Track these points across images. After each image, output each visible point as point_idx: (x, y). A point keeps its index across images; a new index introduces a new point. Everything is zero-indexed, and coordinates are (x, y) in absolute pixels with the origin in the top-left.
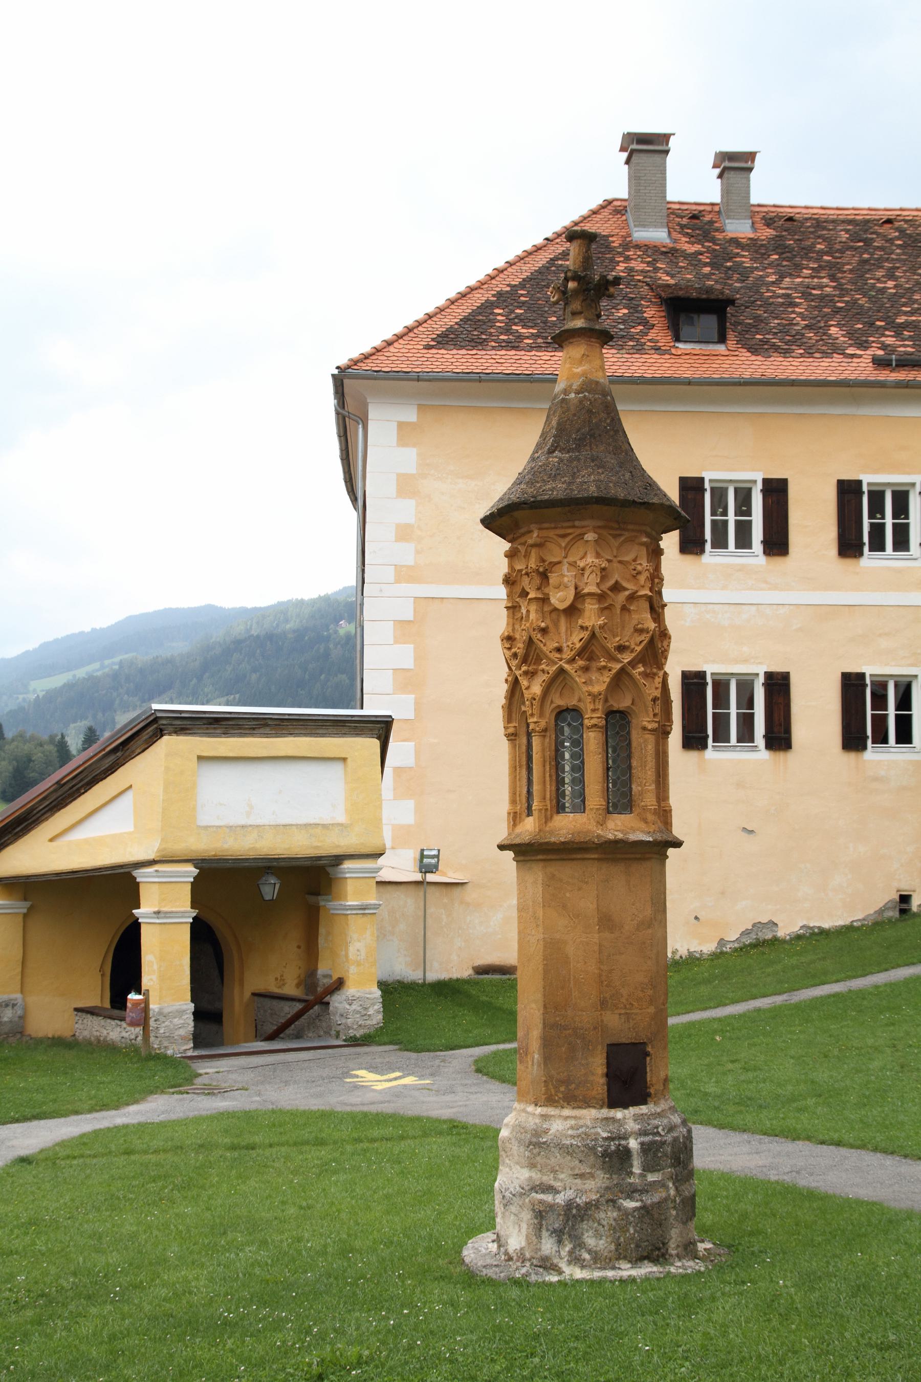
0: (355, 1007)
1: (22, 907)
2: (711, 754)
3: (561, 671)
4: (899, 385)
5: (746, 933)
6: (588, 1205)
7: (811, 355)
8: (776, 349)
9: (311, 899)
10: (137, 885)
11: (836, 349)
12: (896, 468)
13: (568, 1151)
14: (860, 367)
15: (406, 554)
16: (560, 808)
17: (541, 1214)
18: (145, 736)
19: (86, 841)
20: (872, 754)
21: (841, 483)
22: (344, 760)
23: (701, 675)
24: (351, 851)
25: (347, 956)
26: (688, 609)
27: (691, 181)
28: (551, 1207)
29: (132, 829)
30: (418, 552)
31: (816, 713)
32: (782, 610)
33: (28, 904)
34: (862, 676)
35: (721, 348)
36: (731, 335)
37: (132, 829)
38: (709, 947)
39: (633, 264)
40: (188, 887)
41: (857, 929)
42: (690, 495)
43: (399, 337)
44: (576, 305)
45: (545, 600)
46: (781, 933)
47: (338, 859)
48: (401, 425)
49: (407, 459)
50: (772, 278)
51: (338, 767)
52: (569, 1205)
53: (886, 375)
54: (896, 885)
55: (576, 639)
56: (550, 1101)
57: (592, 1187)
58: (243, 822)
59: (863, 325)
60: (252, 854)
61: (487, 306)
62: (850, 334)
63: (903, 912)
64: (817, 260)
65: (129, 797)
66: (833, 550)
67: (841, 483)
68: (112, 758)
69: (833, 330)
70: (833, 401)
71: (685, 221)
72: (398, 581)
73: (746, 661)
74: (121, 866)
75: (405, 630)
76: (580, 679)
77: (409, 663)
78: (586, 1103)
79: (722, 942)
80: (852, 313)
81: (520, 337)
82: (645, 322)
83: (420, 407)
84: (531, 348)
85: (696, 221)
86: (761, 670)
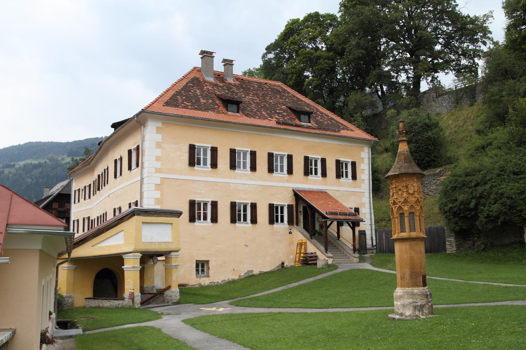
0: (174, 294)
1: (73, 267)
2: (237, 224)
3: (400, 206)
5: (246, 273)
6: (424, 305)
7: (219, 113)
8: (252, 116)
10: (123, 259)
11: (265, 118)
12: (281, 151)
13: (419, 295)
14: (272, 123)
15: (158, 165)
16: (411, 231)
17: (415, 307)
18: (129, 216)
19: (106, 246)
20: (276, 225)
21: (231, 149)
22: (172, 224)
23: (235, 203)
25: (172, 280)
26: (232, 185)
27: (218, 67)
28: (417, 306)
29: (123, 242)
30: (161, 164)
31: (263, 214)
32: (255, 186)
35: (238, 114)
36: (240, 111)
37: (123, 242)
38: (237, 278)
39: (208, 87)
40: (139, 260)
41: (274, 271)
42: (233, 154)
43: (155, 102)
44: (404, 135)
45: (408, 191)
46: (254, 273)
48: (157, 128)
49: (159, 137)
50: (243, 96)
51: (170, 226)
52: (421, 305)
53: (279, 126)
54: (281, 260)
55: (414, 199)
56: (413, 286)
57: (424, 302)
58: (150, 241)
59: (271, 112)
60: (153, 250)
61: (174, 95)
62: (267, 114)
63: (282, 267)
64: (252, 92)
66: (267, 171)
68: (117, 222)
69: (263, 112)
70: (267, 132)
72: (156, 172)
73: (246, 199)
74: (119, 254)
75: (158, 187)
76: (403, 207)
77: (159, 196)
78: (420, 286)
79: (240, 276)
80: (266, 109)
82: (217, 105)
83: (162, 123)
84: (191, 109)
85: (219, 76)
86: (250, 202)
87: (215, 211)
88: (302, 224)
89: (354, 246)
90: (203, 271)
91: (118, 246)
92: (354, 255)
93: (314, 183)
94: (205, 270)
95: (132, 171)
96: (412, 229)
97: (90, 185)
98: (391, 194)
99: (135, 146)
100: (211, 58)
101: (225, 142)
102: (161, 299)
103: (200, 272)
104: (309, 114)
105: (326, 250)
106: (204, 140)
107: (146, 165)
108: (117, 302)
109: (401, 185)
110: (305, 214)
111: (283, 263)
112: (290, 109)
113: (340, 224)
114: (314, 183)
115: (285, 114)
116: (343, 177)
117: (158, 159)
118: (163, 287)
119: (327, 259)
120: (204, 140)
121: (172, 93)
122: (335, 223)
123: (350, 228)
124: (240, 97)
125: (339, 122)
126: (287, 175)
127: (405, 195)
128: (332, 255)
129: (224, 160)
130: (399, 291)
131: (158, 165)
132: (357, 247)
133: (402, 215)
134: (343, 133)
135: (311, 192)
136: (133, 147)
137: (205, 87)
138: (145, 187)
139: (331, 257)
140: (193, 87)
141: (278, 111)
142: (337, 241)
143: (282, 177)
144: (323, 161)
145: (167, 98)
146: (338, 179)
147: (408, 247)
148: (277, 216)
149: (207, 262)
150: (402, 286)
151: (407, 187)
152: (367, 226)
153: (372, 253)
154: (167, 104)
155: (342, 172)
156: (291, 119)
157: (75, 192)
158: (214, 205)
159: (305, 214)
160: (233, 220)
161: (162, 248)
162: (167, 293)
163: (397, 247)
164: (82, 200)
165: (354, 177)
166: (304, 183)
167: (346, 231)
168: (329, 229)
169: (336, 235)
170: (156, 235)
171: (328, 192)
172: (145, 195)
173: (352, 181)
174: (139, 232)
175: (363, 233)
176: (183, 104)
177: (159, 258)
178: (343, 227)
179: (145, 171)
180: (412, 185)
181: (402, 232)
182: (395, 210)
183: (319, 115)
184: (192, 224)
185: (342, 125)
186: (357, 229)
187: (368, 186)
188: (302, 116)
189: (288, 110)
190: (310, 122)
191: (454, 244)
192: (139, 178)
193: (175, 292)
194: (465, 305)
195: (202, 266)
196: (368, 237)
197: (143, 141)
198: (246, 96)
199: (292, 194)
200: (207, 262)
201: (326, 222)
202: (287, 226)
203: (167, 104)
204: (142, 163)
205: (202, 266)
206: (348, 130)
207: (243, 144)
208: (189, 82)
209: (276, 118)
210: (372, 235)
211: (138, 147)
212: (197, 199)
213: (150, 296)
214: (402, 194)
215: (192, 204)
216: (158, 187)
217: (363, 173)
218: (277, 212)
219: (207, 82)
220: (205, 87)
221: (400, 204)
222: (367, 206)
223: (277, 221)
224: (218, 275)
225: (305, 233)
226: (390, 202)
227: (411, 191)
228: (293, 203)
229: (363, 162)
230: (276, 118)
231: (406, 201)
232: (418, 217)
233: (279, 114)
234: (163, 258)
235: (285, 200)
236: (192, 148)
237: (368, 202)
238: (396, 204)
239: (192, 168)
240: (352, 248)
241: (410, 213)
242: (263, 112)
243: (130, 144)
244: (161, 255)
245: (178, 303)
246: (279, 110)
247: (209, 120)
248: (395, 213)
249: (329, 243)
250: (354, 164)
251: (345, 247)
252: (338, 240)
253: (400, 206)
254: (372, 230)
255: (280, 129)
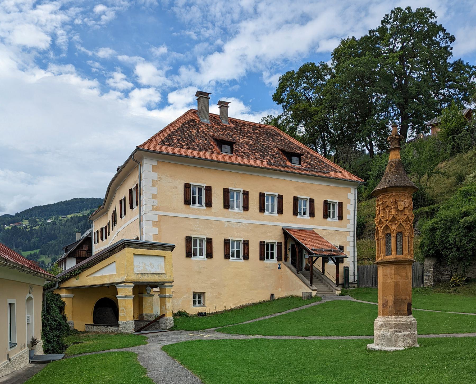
0: (168, 321)
3: (386, 225)
4: (275, 170)
7: (213, 153)
9: (140, 295)
14: (264, 164)
15: (156, 202)
18: (120, 247)
19: (100, 277)
21: (260, 193)
22: (165, 257)
24: (167, 281)
25: (166, 308)
26: (226, 223)
31: (254, 250)
32: (247, 225)
33: (73, 295)
34: (264, 242)
42: (226, 193)
45: (397, 208)
47: (164, 282)
49: (155, 175)
51: (163, 258)
53: (271, 167)
55: (404, 218)
56: (396, 315)
59: (264, 153)
62: (260, 155)
65: (114, 264)
66: (258, 211)
67: (260, 193)
68: (109, 253)
69: (256, 154)
70: (259, 172)
71: (212, 119)
73: (239, 237)
75: (156, 224)
76: (390, 226)
78: (404, 315)
81: (183, 145)
82: (212, 145)
87: (210, 247)
88: (290, 261)
89: (337, 280)
90: (200, 303)
91: (111, 276)
92: (337, 288)
93: (302, 222)
94: (202, 301)
95: (133, 210)
96: (400, 250)
97: (106, 226)
98: (377, 212)
99: (135, 186)
100: (207, 99)
101: (218, 182)
102: (156, 326)
103: (197, 302)
104: (299, 156)
105: (311, 283)
106: (200, 179)
107: (144, 202)
108: (113, 328)
109: (389, 200)
110: (293, 251)
111: (272, 295)
112: (282, 151)
113: (325, 260)
114: (302, 222)
115: (277, 156)
116: (330, 217)
117: (155, 197)
118: (159, 314)
119: (311, 291)
120: (200, 179)
121: (168, 132)
122: (321, 258)
123: (334, 264)
124: (234, 139)
125: (328, 165)
126: (277, 215)
127: (393, 212)
128: (316, 288)
129: (217, 199)
130: (379, 320)
131: (156, 202)
132: (340, 281)
133: (388, 236)
134: (332, 174)
135: (299, 230)
136: (133, 187)
137: (201, 129)
138: (144, 223)
139: (316, 290)
140: (188, 128)
141: (270, 153)
142: (322, 276)
143: (272, 216)
144: (312, 201)
145: (161, 138)
146: (325, 219)
147: (393, 272)
148: (267, 253)
149: (204, 293)
150: (383, 315)
151: (396, 203)
152: (350, 262)
153: (354, 287)
154: (162, 143)
155: (330, 212)
156: (282, 160)
157: (95, 234)
158: (209, 241)
159: (293, 251)
160: (227, 256)
161: (155, 279)
162: (162, 320)
163: (381, 271)
164: (100, 240)
165: (340, 218)
166: (292, 222)
167: (330, 266)
168: (314, 264)
169: (321, 270)
170: (147, 267)
171: (315, 231)
172: (144, 230)
173: (338, 221)
174: (131, 264)
175: (346, 270)
176: (178, 143)
177: (154, 289)
178: (328, 264)
179: (143, 208)
180: (402, 201)
181: (387, 255)
182: (381, 230)
183: (310, 158)
184: (188, 259)
185: (331, 167)
186: (341, 266)
187: (353, 226)
188: (293, 158)
189: (280, 152)
190: (300, 164)
191: (432, 279)
192: (138, 216)
193: (169, 319)
194: (457, 335)
195: (198, 297)
196: (351, 273)
197: (141, 180)
198: (240, 138)
199: (282, 232)
200: (204, 293)
201: (312, 257)
202: (277, 262)
203: (162, 143)
204: (141, 201)
205: (198, 297)
206: (336, 172)
207: (237, 183)
208: (185, 123)
209: (268, 159)
210: (354, 270)
211: (137, 185)
212: (193, 236)
213: (147, 323)
214: (389, 212)
215: (188, 240)
216: (156, 224)
217: (349, 214)
218: (267, 249)
219: (203, 124)
220: (201, 129)
221: (386, 223)
222: (351, 244)
223: (267, 258)
224: (210, 306)
225: (293, 268)
226: (376, 221)
227: (401, 208)
228: (283, 241)
229: (350, 203)
230: (268, 159)
231: (394, 220)
232: (407, 238)
233: (271, 155)
234: (158, 289)
235: (274, 237)
236: (187, 186)
237: (352, 240)
238: (382, 223)
239: (188, 206)
240: (335, 282)
241: (398, 233)
242: (256, 154)
243: (130, 184)
244: (156, 286)
245: (171, 329)
246: (271, 152)
247: (203, 159)
248: (380, 234)
249: (312, 276)
250: (340, 205)
251: (329, 281)
252: (323, 275)
253: (386, 225)
254: (354, 266)
255: (271, 169)
